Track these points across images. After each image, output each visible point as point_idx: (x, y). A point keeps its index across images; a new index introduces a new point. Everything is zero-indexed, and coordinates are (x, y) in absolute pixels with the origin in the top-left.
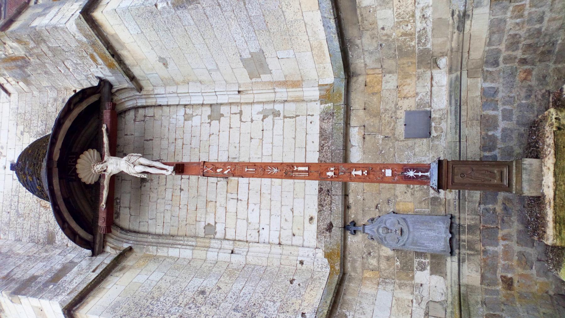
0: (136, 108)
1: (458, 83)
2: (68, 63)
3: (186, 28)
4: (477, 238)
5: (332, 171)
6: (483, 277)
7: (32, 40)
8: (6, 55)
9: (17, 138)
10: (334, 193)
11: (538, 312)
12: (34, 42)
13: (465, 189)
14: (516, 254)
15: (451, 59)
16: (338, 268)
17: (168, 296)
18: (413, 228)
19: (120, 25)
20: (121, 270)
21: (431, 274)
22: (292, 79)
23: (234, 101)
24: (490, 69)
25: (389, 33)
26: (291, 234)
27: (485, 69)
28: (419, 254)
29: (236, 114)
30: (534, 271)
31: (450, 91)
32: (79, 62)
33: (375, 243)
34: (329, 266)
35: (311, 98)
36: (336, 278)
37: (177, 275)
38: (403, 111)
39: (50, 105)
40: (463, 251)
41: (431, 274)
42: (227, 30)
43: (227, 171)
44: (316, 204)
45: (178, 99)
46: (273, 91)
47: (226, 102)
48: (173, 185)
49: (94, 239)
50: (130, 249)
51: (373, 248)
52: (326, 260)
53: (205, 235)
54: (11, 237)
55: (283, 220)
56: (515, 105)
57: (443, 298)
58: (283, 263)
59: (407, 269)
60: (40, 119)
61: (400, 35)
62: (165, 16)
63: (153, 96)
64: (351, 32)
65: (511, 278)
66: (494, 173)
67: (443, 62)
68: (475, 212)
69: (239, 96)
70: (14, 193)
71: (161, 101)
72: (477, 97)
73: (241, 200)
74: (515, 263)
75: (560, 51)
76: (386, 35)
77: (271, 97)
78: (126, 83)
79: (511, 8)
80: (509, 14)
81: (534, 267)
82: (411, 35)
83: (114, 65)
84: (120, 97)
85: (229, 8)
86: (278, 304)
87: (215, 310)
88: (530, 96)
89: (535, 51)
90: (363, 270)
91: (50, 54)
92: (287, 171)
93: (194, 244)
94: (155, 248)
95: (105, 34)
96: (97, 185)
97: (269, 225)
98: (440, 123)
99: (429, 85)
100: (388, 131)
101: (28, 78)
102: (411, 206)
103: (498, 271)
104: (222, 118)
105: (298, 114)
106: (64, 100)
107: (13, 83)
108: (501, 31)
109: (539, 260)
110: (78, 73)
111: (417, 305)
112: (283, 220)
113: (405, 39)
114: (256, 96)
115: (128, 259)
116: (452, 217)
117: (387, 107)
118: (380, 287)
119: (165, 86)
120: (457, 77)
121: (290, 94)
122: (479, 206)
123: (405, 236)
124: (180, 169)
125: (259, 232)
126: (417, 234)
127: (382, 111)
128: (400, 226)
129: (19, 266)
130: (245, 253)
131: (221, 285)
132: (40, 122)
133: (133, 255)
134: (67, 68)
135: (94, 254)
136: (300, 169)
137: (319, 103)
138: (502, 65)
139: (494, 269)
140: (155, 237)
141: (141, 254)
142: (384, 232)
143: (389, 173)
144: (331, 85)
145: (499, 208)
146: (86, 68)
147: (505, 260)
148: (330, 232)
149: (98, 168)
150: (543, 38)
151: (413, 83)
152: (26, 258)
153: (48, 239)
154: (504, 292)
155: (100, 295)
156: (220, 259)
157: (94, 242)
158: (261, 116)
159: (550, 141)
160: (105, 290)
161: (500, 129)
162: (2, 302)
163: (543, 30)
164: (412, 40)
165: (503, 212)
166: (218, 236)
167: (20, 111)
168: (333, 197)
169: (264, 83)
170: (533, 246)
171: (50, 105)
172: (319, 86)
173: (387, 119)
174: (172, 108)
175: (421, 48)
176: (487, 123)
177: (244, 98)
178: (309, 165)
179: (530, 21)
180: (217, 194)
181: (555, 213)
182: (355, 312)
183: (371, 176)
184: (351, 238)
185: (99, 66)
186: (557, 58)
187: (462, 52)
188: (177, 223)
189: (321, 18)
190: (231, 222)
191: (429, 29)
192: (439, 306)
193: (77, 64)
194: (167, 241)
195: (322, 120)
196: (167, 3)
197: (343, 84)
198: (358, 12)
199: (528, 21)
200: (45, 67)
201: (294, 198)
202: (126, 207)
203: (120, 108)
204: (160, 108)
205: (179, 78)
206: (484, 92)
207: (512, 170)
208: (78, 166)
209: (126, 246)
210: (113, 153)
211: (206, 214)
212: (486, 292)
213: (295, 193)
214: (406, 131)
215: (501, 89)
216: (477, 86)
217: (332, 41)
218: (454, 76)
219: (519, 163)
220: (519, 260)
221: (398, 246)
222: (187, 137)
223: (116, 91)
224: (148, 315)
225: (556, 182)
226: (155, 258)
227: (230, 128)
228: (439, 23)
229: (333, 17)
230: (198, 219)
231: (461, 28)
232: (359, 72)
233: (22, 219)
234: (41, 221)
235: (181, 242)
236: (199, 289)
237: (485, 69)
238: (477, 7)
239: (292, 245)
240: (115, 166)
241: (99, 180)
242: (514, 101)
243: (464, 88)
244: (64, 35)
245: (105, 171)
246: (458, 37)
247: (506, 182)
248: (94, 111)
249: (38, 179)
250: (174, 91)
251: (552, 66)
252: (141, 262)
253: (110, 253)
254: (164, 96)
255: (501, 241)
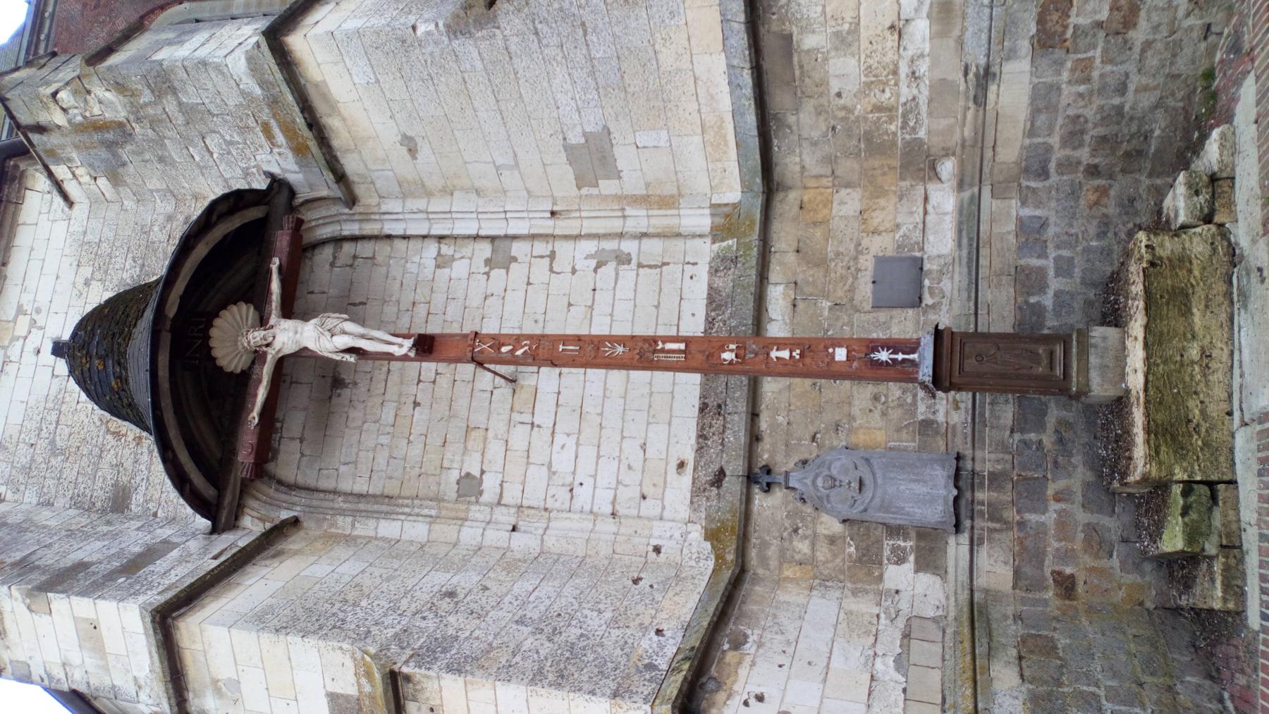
0: (339, 240)
1: (975, 208)
2: (212, 142)
3: (466, 75)
4: (1007, 497)
5: (732, 351)
6: (1017, 574)
7: (149, 86)
8: (85, 117)
9: (76, 292)
10: (730, 409)
11: (1124, 633)
12: (153, 92)
13: (983, 391)
14: (1080, 529)
15: (962, 164)
16: (730, 557)
17: (377, 598)
18: (884, 478)
19: (336, 63)
20: (274, 556)
21: (916, 571)
22: (659, 192)
23: (541, 231)
24: (1033, 184)
25: (849, 104)
26: (638, 495)
27: (1025, 183)
28: (895, 531)
29: (542, 257)
30: (1115, 562)
31: (960, 223)
32: (237, 138)
33: (808, 509)
34: (713, 556)
35: (694, 230)
36: (727, 575)
37: (396, 566)
38: (870, 257)
39: (156, 228)
40: (979, 523)
41: (916, 571)
42: (545, 84)
43: (522, 351)
44: (693, 435)
45: (427, 225)
46: (620, 214)
47: (525, 232)
48: (400, 395)
49: (220, 497)
50: (295, 522)
51: (803, 520)
52: (708, 545)
53: (459, 496)
54: (30, 498)
55: (624, 468)
56: (1079, 249)
57: (940, 613)
58: (618, 550)
59: (868, 563)
60: (130, 255)
61: (869, 109)
62: (429, 49)
63: (377, 217)
64: (779, 100)
65: (1072, 576)
66: (1038, 354)
67: (948, 168)
68: (1003, 447)
69: (551, 223)
70: (50, 405)
71: (389, 228)
72: (1009, 233)
73: (539, 426)
74: (1078, 545)
75: (1158, 151)
76: (844, 108)
77: (616, 225)
78: (324, 186)
79: (1069, 65)
80: (1065, 75)
81: (1115, 553)
82: (890, 110)
83: (307, 147)
84: (309, 215)
85: (555, 40)
86: (608, 615)
87: (477, 622)
88: (1105, 233)
89: (1113, 150)
90: (781, 564)
91: (180, 120)
92: (643, 353)
93: (433, 512)
94: (349, 519)
95: (303, 82)
96: (244, 380)
97: (595, 476)
98: (940, 281)
99: (921, 210)
100: (840, 293)
101: (120, 170)
102: (880, 436)
103: (1047, 563)
104: (513, 266)
105: (666, 260)
106: (187, 218)
107: (86, 179)
108: (1052, 108)
109: (1125, 541)
110: (228, 164)
111: (888, 622)
112: (624, 468)
113: (879, 119)
114: (585, 223)
115: (290, 539)
116: (959, 458)
117: (841, 249)
118: (815, 592)
119: (404, 196)
120: (972, 197)
121: (653, 221)
122: (1011, 436)
123: (868, 493)
124: (426, 346)
125: (571, 490)
126: (891, 490)
127: (831, 255)
128: (858, 474)
129: (49, 546)
130: (541, 531)
131: (489, 584)
132: (130, 261)
133: (302, 533)
134: (208, 150)
135: (215, 530)
136: (670, 346)
137: (709, 240)
138: (1054, 178)
139: (1038, 557)
140: (350, 498)
141: (318, 533)
142: (827, 485)
143: (841, 354)
144: (734, 206)
145: (1048, 440)
146: (247, 152)
147: (1060, 540)
148: (718, 487)
149: (256, 336)
150: (1128, 125)
151: (891, 207)
152: (64, 533)
153: (114, 502)
154: (1058, 602)
155: (231, 595)
156: (487, 542)
157: (219, 505)
158: (593, 263)
159: (1137, 288)
160: (241, 588)
161: (1051, 293)
162: (7, 606)
163: (1127, 108)
164: (891, 120)
165: (1056, 447)
166: (486, 498)
167: (89, 237)
168: (729, 418)
169: (605, 198)
170: (1114, 511)
171: (156, 228)
172: (712, 206)
173: (840, 271)
174: (412, 243)
175: (908, 137)
176: (1028, 281)
177: (562, 226)
178: (687, 340)
179: (1102, 91)
180: (490, 412)
181: (1147, 415)
182: (764, 629)
183: (808, 360)
184: (759, 499)
185: (276, 150)
186: (1153, 165)
187: (982, 148)
188: (400, 471)
189: (725, 68)
190: (514, 471)
191: (923, 100)
192: (932, 626)
193: (230, 143)
194: (376, 507)
195: (714, 271)
196: (437, 25)
197: (759, 202)
198: (795, 59)
199: (1099, 90)
200: (163, 146)
201: (649, 423)
202: (293, 439)
203: (308, 238)
204: (388, 241)
205: (434, 182)
206: (1022, 224)
207: (1071, 348)
208: (214, 332)
209: (285, 515)
210: (288, 312)
211: (464, 454)
212: (1023, 601)
213: (652, 413)
214: (874, 293)
215: (1052, 220)
216: (1009, 213)
217: (743, 114)
218: (966, 195)
219: (1083, 335)
220: (1088, 541)
221: (854, 513)
222: (439, 298)
223: (302, 204)
224: (334, 627)
225: (1147, 358)
226: (349, 540)
227: (529, 283)
228: (941, 89)
229: (748, 65)
230: (446, 464)
231: (981, 99)
232: (789, 183)
233: (60, 458)
234: (104, 465)
235: (407, 510)
236: (444, 589)
237: (1025, 183)
238: (1008, 59)
239: (639, 517)
240: (291, 334)
241: (251, 368)
242: (1077, 241)
243: (985, 216)
244: (218, 80)
245: (268, 345)
246: (976, 117)
247: (1059, 371)
248: (252, 240)
249: (119, 364)
250: (422, 207)
251: (1145, 181)
252: (319, 545)
253: (252, 526)
254: (401, 217)
255: (1052, 502)
